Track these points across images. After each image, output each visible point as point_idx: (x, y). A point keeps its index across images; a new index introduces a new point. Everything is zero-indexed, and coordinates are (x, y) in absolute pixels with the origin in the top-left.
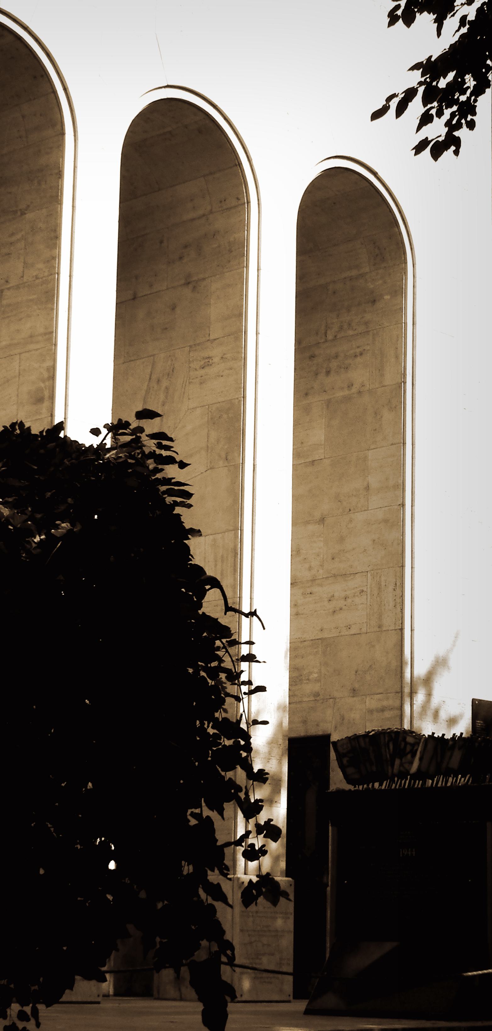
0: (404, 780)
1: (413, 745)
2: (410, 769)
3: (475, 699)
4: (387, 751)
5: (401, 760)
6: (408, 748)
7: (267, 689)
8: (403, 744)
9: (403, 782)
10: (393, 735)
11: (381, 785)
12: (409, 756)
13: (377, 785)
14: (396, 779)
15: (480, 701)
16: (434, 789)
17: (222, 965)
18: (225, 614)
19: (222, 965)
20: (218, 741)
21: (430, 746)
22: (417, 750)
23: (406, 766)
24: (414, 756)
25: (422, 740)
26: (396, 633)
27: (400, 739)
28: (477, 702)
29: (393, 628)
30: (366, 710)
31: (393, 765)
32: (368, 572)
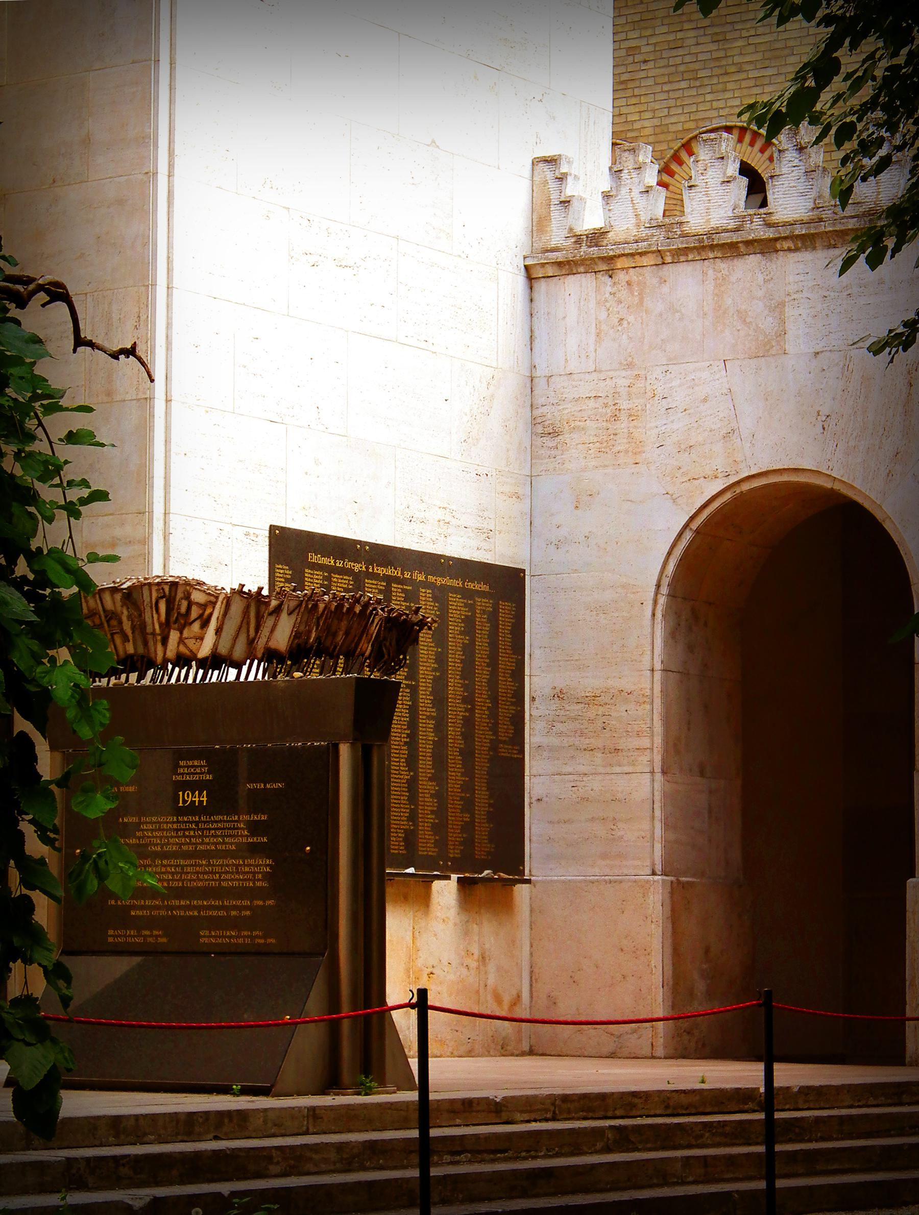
0: (186, 668)
1: (203, 606)
3: (274, 526)
4: (155, 616)
5: (181, 633)
6: (195, 613)
8: (185, 604)
9: (184, 672)
10: (167, 588)
11: (141, 677)
12: (196, 626)
13: (133, 677)
15: (283, 529)
16: (221, 686)
18: (75, 351)
21: (237, 607)
22: (211, 615)
23: (191, 643)
24: (205, 624)
25: (221, 599)
26: (139, 407)
27: (180, 594)
32: (88, 295)
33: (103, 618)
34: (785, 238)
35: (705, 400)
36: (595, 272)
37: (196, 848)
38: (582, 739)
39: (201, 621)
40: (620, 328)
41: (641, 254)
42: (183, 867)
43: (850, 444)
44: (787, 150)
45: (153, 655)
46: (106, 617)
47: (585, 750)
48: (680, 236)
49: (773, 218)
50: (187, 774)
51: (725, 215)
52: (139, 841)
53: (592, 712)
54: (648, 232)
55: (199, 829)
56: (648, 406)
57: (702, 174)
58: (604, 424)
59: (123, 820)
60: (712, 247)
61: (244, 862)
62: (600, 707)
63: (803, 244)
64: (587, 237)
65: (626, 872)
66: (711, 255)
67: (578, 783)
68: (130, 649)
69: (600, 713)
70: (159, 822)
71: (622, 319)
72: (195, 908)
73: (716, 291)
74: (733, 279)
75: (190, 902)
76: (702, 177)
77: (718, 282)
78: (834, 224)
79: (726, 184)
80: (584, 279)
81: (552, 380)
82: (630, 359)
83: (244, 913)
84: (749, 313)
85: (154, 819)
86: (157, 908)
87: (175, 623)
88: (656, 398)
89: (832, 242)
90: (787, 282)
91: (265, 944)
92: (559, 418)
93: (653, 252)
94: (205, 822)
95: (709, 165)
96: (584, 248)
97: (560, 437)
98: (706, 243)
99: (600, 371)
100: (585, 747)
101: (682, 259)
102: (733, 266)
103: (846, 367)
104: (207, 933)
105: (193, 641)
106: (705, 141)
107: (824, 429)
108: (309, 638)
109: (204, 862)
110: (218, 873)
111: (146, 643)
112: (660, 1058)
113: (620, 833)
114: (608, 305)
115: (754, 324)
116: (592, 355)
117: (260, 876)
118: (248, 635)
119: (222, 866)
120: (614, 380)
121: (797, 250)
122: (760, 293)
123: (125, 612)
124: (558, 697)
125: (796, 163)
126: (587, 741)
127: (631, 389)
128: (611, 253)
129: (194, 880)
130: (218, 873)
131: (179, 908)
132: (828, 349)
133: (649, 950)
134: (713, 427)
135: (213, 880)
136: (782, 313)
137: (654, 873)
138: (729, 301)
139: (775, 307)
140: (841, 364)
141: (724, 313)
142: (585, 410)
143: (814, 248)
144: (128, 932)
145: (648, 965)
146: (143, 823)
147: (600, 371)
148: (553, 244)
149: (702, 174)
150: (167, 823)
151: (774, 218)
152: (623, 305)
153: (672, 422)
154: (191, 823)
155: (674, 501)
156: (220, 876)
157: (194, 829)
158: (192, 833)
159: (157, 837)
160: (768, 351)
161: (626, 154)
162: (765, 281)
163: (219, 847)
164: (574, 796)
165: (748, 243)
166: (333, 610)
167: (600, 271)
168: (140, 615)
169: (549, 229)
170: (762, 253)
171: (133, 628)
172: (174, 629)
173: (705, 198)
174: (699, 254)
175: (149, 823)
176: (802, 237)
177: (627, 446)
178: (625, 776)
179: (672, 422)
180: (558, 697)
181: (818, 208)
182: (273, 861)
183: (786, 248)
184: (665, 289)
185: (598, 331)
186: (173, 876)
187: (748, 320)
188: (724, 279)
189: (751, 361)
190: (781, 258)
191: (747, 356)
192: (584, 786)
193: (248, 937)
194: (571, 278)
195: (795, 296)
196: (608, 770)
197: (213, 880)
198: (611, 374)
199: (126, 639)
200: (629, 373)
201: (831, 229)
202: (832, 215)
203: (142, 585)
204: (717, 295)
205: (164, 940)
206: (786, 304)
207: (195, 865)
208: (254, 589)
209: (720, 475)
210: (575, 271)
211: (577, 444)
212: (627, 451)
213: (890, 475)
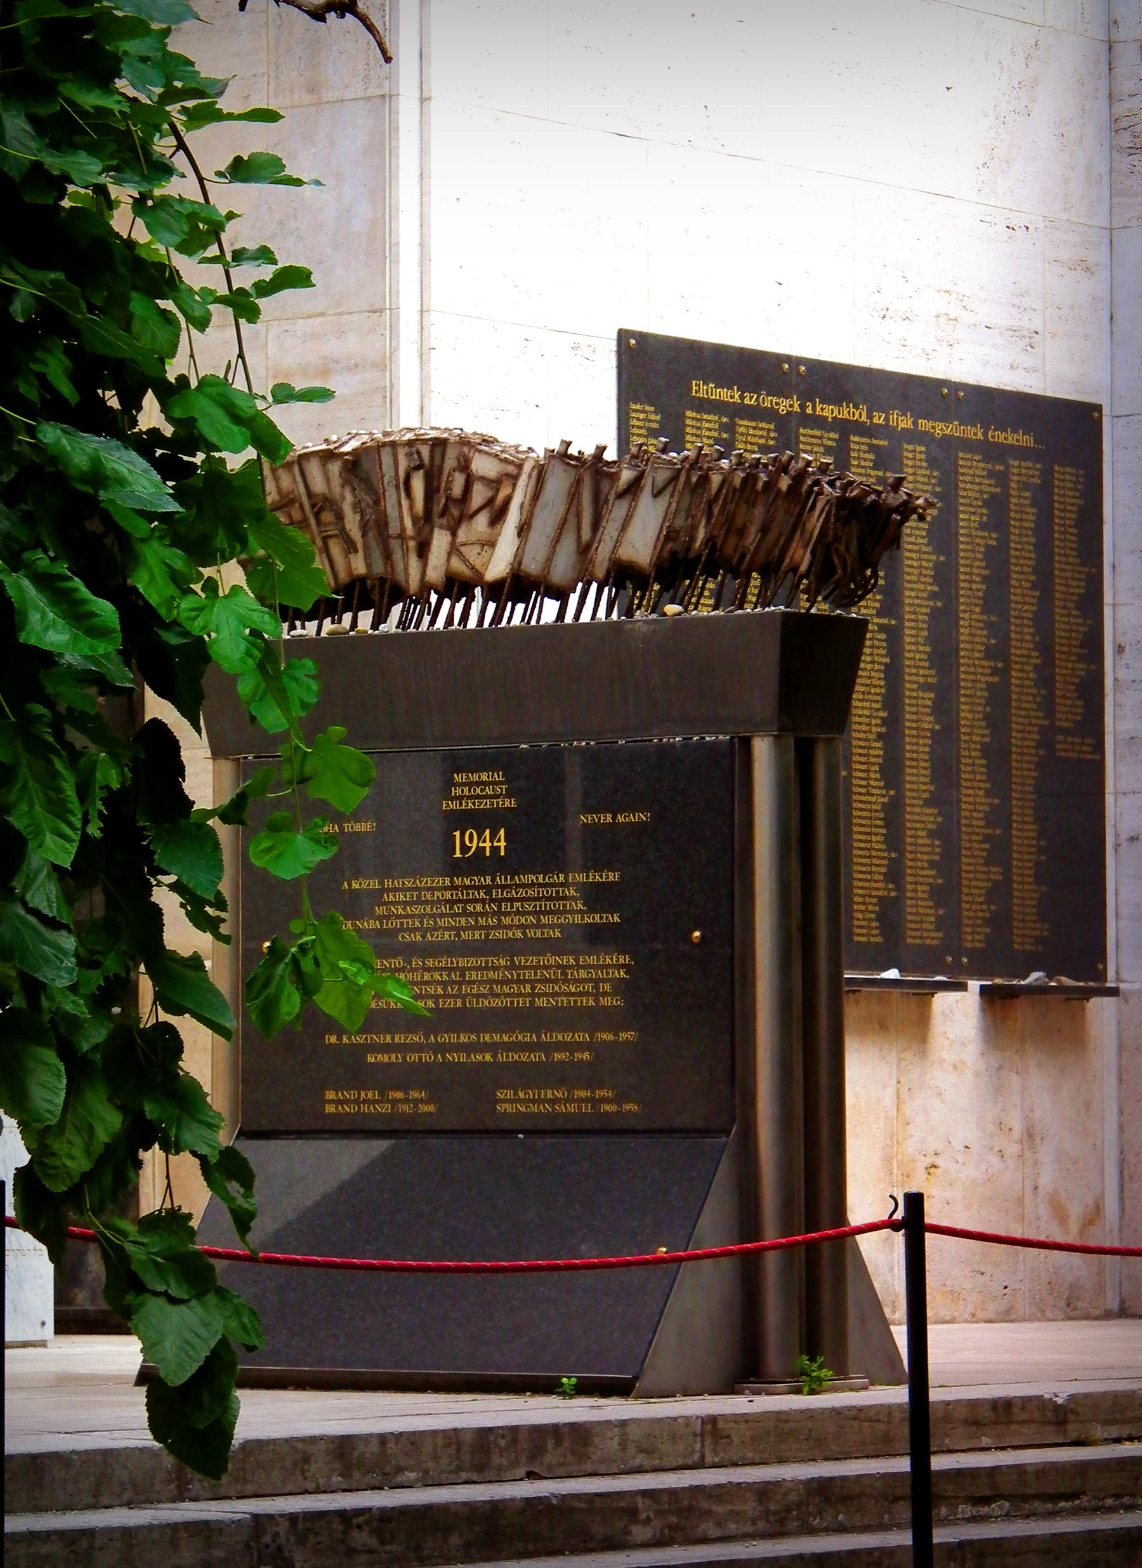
0: (464, 599)
1: (494, 484)
2: (486, 565)
3: (627, 331)
4: (405, 503)
6: (479, 495)
7: (314, 278)
9: (459, 607)
10: (425, 451)
12: (481, 522)
14: (434, 598)
17: (927, 1234)
19: (927, 1234)
20: (186, 458)
21: (558, 484)
24: (498, 517)
25: (527, 468)
28: (633, 342)
29: (360, 94)
30: (267, 369)
31: (423, 550)
33: (307, 508)
37: (487, 935)
45: (401, 577)
46: (313, 506)
55: (492, 900)
59: (350, 885)
86: (419, 1048)
91: (619, 1113)
94: (503, 887)
104: (510, 1094)
108: (692, 539)
111: (388, 556)
117: (608, 987)
118: (579, 537)
129: (484, 996)
130: (529, 981)
144: (363, 1094)
154: (478, 888)
157: (483, 901)
158: (479, 908)
163: (530, 933)
168: (377, 502)
171: (364, 528)
172: (441, 527)
182: (631, 959)
193: (586, 1100)
197: (520, 995)
199: (350, 546)
203: (379, 447)
205: (430, 1108)
207: (486, 968)
208: (589, 451)
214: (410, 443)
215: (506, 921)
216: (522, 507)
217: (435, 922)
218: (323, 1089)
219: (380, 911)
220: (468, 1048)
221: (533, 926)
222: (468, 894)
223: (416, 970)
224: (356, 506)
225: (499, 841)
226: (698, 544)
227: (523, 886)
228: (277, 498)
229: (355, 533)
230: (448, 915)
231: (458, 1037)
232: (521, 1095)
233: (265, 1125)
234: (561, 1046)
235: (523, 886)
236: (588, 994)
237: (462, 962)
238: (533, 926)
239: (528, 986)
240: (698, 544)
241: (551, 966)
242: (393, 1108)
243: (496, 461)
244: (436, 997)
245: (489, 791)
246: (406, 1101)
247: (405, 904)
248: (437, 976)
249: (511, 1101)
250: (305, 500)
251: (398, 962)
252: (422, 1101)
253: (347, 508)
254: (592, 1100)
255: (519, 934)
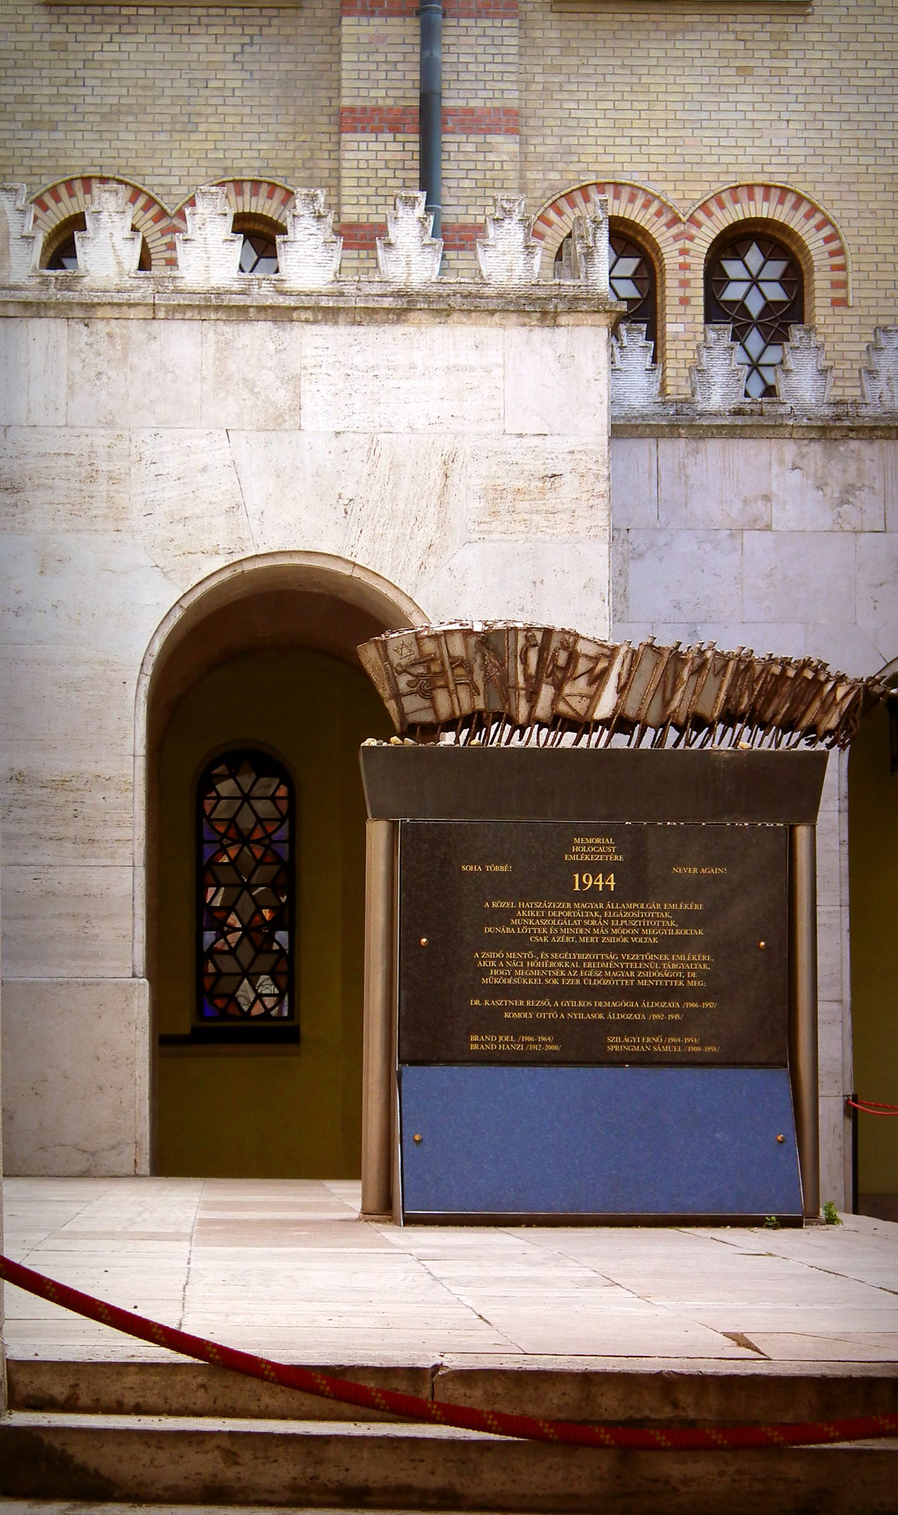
6: (583, 665)
10: (539, 636)
25: (622, 651)
33: (447, 664)
34: (306, 308)
35: (204, 470)
36: (67, 319)
37: (600, 940)
38: (48, 827)
39: (590, 676)
40: (98, 382)
41: (130, 305)
42: (581, 962)
43: (377, 531)
44: (303, 216)
45: (514, 712)
46: (451, 664)
47: (51, 839)
48: (172, 292)
49: (287, 286)
50: (585, 853)
51: (229, 276)
52: (516, 930)
53: (59, 799)
54: (132, 282)
55: (604, 918)
56: (133, 470)
57: (200, 228)
58: (78, 485)
59: (490, 904)
60: (218, 308)
61: (670, 957)
62: (71, 793)
63: (324, 316)
64: (57, 279)
65: (101, 973)
66: (213, 316)
67: (42, 876)
68: (480, 704)
69: (70, 799)
70: (544, 909)
71: (100, 373)
72: (600, 1010)
73: (218, 355)
74: (238, 344)
75: (593, 1004)
76: (199, 232)
77: (220, 346)
78: (367, 301)
79: (229, 243)
80: (52, 325)
81: (10, 431)
82: (110, 417)
83: (671, 1017)
84: (258, 383)
85: (538, 905)
86: (546, 1009)
87: (548, 677)
88: (143, 462)
89: (358, 319)
90: (303, 354)
91: (702, 1052)
92: (19, 474)
93: (146, 305)
94: (612, 910)
95: (209, 220)
96: (52, 290)
97: (22, 494)
98: (214, 302)
99: (73, 427)
100: (52, 835)
101: (178, 316)
102: (239, 331)
103: (372, 452)
104: (618, 1039)
105: (578, 699)
106: (204, 194)
107: (346, 513)
108: (739, 703)
109: (612, 957)
110: (632, 970)
111: (507, 700)
112: (144, 1176)
113: (96, 931)
114: (83, 356)
115: (263, 395)
116: (63, 408)
117: (694, 975)
118: (664, 697)
119: (638, 962)
120: (90, 439)
121: (315, 322)
122: (271, 363)
123: (479, 660)
124: (17, 780)
125: (313, 230)
126: (54, 830)
127: (111, 450)
128: (96, 300)
129: (599, 978)
130: (632, 970)
131: (578, 1010)
132: (352, 430)
133: (132, 1060)
134: (214, 499)
135: (626, 978)
136: (297, 386)
137: (134, 976)
138: (233, 368)
139: (290, 380)
140: (367, 447)
141: (228, 379)
142: (53, 467)
143: (336, 323)
144: (501, 1038)
145: (131, 1075)
146: (521, 909)
147: (73, 427)
148: (13, 281)
149: (200, 228)
150: (557, 910)
151: (287, 286)
152: (102, 358)
153: (163, 489)
154: (593, 911)
155: (165, 574)
156: (636, 974)
157: (597, 919)
158: (593, 923)
159: (543, 926)
160: (279, 425)
161: (107, 195)
162: (277, 351)
163: (634, 940)
164: (37, 889)
165: (261, 309)
166: (533, 673)
167: (73, 318)
168: (503, 665)
169: (7, 265)
170: (274, 321)
171: (487, 680)
172: (547, 684)
173: (202, 254)
174: (199, 313)
175: (530, 909)
176: (326, 310)
177: (106, 511)
178: (102, 869)
179: (163, 489)
180: (17, 780)
181: (339, 281)
182: (711, 958)
183: (303, 319)
184: (155, 346)
185: (70, 383)
186: (566, 973)
187: (256, 390)
188: (227, 343)
189: (259, 434)
190: (296, 329)
191: (254, 428)
192: (50, 879)
193: (677, 1044)
194: (36, 322)
195: (313, 371)
196: (80, 862)
197: (626, 978)
198: (86, 431)
199: (475, 691)
200: (110, 432)
201: (363, 305)
202: (355, 291)
203: (509, 630)
204: (219, 359)
205: (556, 1048)
206: (303, 378)
207: (600, 960)
208: (671, 645)
209: (221, 552)
210: (43, 315)
211: (43, 504)
212: (106, 517)
213: (423, 567)
214: (528, 630)
215: (616, 931)
216: (619, 675)
217: (559, 931)
218: (468, 1035)
219: (515, 922)
220: (634, 1011)
221: (636, 935)
222: (585, 914)
223: (544, 960)
224: (484, 667)
225: (610, 881)
226: (743, 707)
227: (628, 910)
228: (418, 657)
229: (480, 684)
230: (569, 927)
231: (577, 1003)
232: (627, 1040)
233: (420, 1056)
234: (657, 1010)
235: (628, 910)
236: (679, 978)
237: (580, 956)
238: (636, 935)
239: (632, 974)
240: (743, 707)
241: (650, 961)
242: (524, 1047)
243: (595, 646)
244: (560, 978)
245: (601, 850)
246: (536, 1043)
247: (535, 918)
248: (560, 964)
249: (619, 1044)
250: (446, 659)
251: (530, 954)
252: (548, 1043)
253: (476, 667)
254: (682, 1044)
255: (625, 940)
